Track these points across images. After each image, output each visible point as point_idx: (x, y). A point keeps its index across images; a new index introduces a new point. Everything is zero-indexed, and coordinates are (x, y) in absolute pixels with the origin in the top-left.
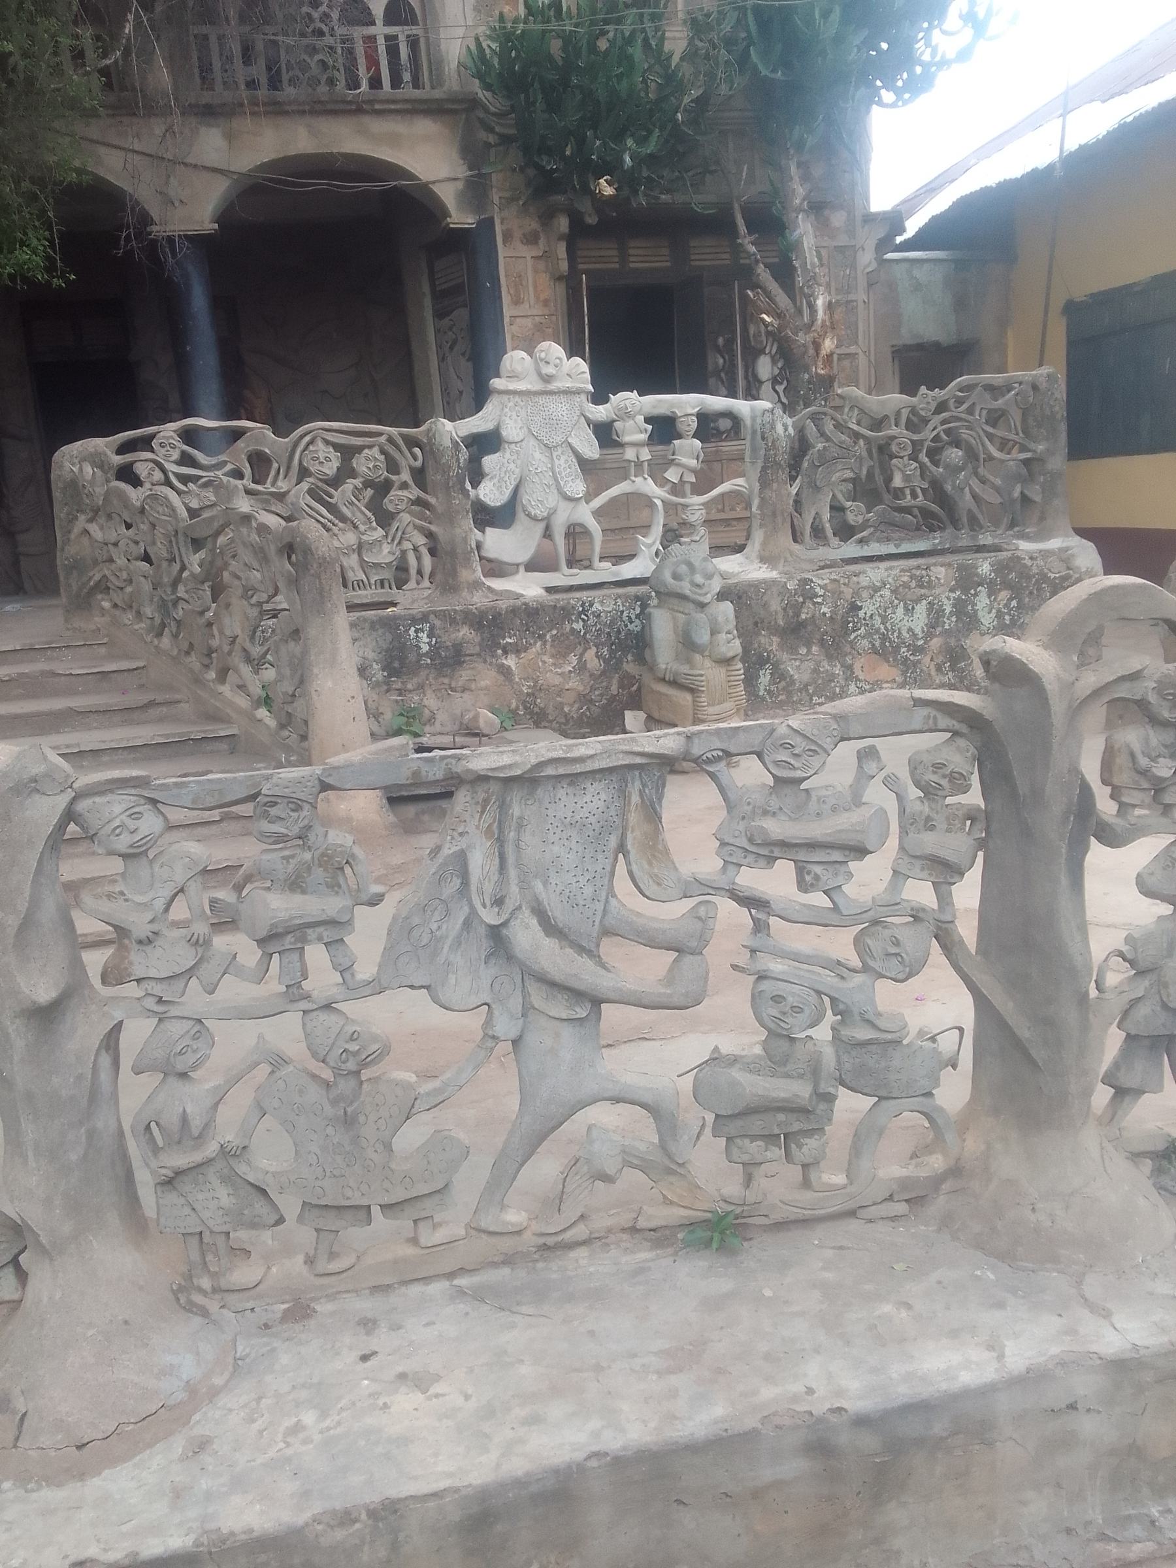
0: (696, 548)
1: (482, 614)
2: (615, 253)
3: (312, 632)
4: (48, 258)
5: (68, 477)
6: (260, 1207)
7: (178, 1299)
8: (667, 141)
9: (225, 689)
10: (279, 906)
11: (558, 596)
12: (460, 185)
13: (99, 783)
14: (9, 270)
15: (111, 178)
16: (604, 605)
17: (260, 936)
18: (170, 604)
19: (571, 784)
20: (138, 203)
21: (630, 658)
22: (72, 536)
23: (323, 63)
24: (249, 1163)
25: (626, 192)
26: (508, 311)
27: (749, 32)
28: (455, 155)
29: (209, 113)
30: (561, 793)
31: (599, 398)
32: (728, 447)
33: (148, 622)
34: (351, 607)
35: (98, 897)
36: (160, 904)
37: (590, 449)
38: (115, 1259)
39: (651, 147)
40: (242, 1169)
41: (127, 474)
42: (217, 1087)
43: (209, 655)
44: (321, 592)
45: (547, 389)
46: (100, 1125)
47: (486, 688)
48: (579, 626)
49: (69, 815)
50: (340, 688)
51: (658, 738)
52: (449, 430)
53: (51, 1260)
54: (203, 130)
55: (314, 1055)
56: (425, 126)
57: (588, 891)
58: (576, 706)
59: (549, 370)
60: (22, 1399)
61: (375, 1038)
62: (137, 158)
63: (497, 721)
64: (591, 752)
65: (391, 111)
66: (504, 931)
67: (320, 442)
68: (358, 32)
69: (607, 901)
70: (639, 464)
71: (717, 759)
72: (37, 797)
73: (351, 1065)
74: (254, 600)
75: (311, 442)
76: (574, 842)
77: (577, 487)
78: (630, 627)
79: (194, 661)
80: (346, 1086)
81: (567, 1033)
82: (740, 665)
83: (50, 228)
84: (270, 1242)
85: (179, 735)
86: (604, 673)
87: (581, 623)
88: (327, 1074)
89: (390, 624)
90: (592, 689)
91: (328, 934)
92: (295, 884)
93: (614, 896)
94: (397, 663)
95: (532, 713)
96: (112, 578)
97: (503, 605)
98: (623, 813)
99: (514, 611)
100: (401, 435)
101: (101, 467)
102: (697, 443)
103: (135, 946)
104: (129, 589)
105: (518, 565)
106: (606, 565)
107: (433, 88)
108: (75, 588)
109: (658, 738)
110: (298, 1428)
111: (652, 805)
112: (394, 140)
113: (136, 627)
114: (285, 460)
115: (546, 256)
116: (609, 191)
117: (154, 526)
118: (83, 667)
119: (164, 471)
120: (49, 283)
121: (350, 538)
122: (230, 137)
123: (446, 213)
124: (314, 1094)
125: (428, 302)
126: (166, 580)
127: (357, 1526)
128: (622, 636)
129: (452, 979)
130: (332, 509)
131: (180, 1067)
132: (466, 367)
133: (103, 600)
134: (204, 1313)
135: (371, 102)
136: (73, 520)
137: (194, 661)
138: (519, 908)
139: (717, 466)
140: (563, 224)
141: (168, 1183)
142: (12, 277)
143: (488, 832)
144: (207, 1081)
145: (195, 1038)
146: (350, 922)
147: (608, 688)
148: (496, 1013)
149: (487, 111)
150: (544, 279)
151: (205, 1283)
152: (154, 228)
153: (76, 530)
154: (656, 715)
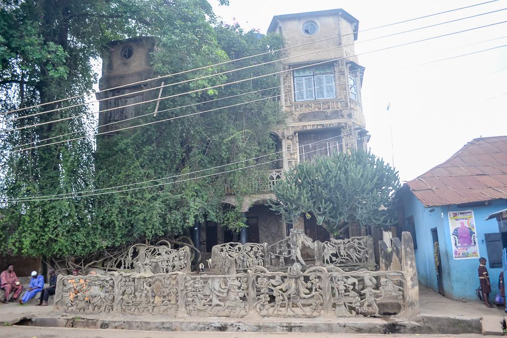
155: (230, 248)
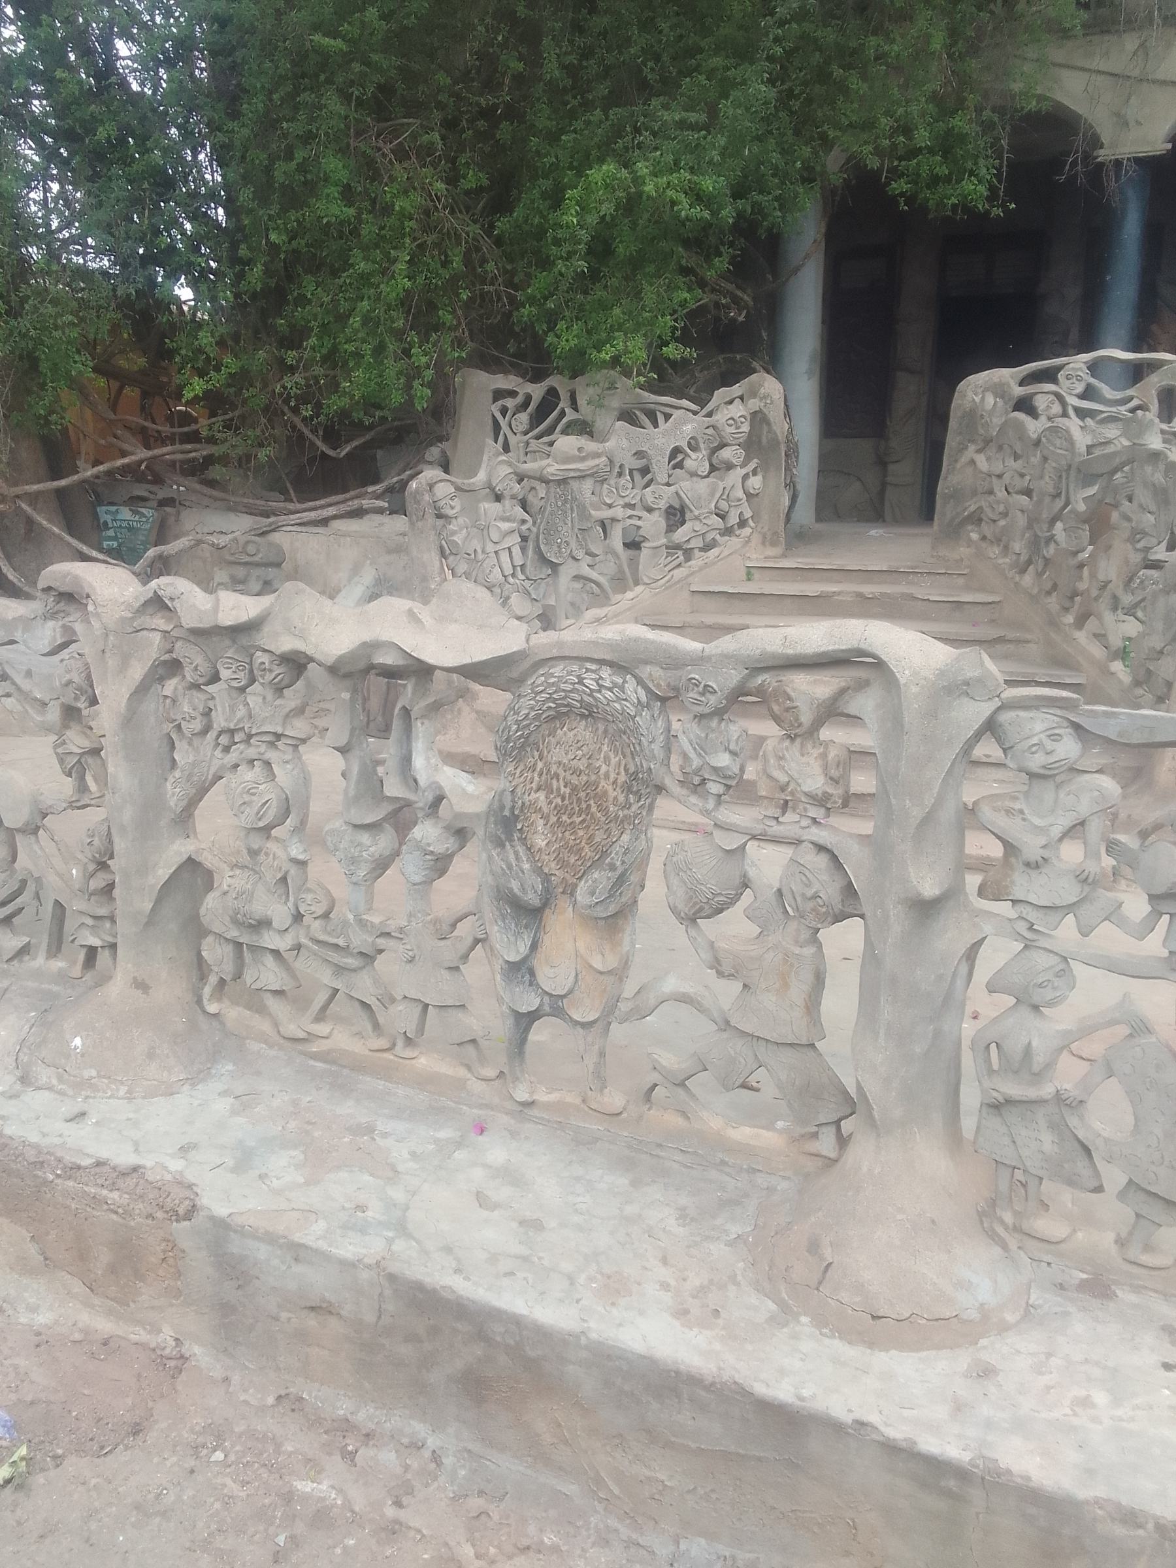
4: (992, 189)
5: (968, 406)
6: (1081, 1165)
7: (982, 1222)
9: (1081, 636)
13: (1028, 697)
14: (954, 200)
15: (1067, 102)
17: (1153, 892)
18: (1043, 541)
20: (1091, 127)
22: (958, 466)
24: (1081, 1118)
33: (1014, 557)
35: (995, 809)
36: (1056, 832)
38: (930, 1158)
40: (1073, 1122)
41: (1025, 405)
43: (1072, 598)
49: (990, 727)
53: (878, 1135)
60: (829, 1250)
72: (965, 700)
74: (1140, 545)
79: (1053, 603)
84: (1070, 1205)
96: (988, 510)
101: (1002, 397)
110: (1086, 1402)
113: (1000, 561)
118: (940, 595)
119: (1064, 403)
120: (988, 212)
127: (1141, 1532)
131: (1036, 999)
133: (972, 531)
134: (1005, 1247)
136: (962, 449)
137: (1053, 603)
142: (954, 206)
145: (1057, 976)
151: (1008, 1218)
152: (1102, 152)
153: (964, 460)
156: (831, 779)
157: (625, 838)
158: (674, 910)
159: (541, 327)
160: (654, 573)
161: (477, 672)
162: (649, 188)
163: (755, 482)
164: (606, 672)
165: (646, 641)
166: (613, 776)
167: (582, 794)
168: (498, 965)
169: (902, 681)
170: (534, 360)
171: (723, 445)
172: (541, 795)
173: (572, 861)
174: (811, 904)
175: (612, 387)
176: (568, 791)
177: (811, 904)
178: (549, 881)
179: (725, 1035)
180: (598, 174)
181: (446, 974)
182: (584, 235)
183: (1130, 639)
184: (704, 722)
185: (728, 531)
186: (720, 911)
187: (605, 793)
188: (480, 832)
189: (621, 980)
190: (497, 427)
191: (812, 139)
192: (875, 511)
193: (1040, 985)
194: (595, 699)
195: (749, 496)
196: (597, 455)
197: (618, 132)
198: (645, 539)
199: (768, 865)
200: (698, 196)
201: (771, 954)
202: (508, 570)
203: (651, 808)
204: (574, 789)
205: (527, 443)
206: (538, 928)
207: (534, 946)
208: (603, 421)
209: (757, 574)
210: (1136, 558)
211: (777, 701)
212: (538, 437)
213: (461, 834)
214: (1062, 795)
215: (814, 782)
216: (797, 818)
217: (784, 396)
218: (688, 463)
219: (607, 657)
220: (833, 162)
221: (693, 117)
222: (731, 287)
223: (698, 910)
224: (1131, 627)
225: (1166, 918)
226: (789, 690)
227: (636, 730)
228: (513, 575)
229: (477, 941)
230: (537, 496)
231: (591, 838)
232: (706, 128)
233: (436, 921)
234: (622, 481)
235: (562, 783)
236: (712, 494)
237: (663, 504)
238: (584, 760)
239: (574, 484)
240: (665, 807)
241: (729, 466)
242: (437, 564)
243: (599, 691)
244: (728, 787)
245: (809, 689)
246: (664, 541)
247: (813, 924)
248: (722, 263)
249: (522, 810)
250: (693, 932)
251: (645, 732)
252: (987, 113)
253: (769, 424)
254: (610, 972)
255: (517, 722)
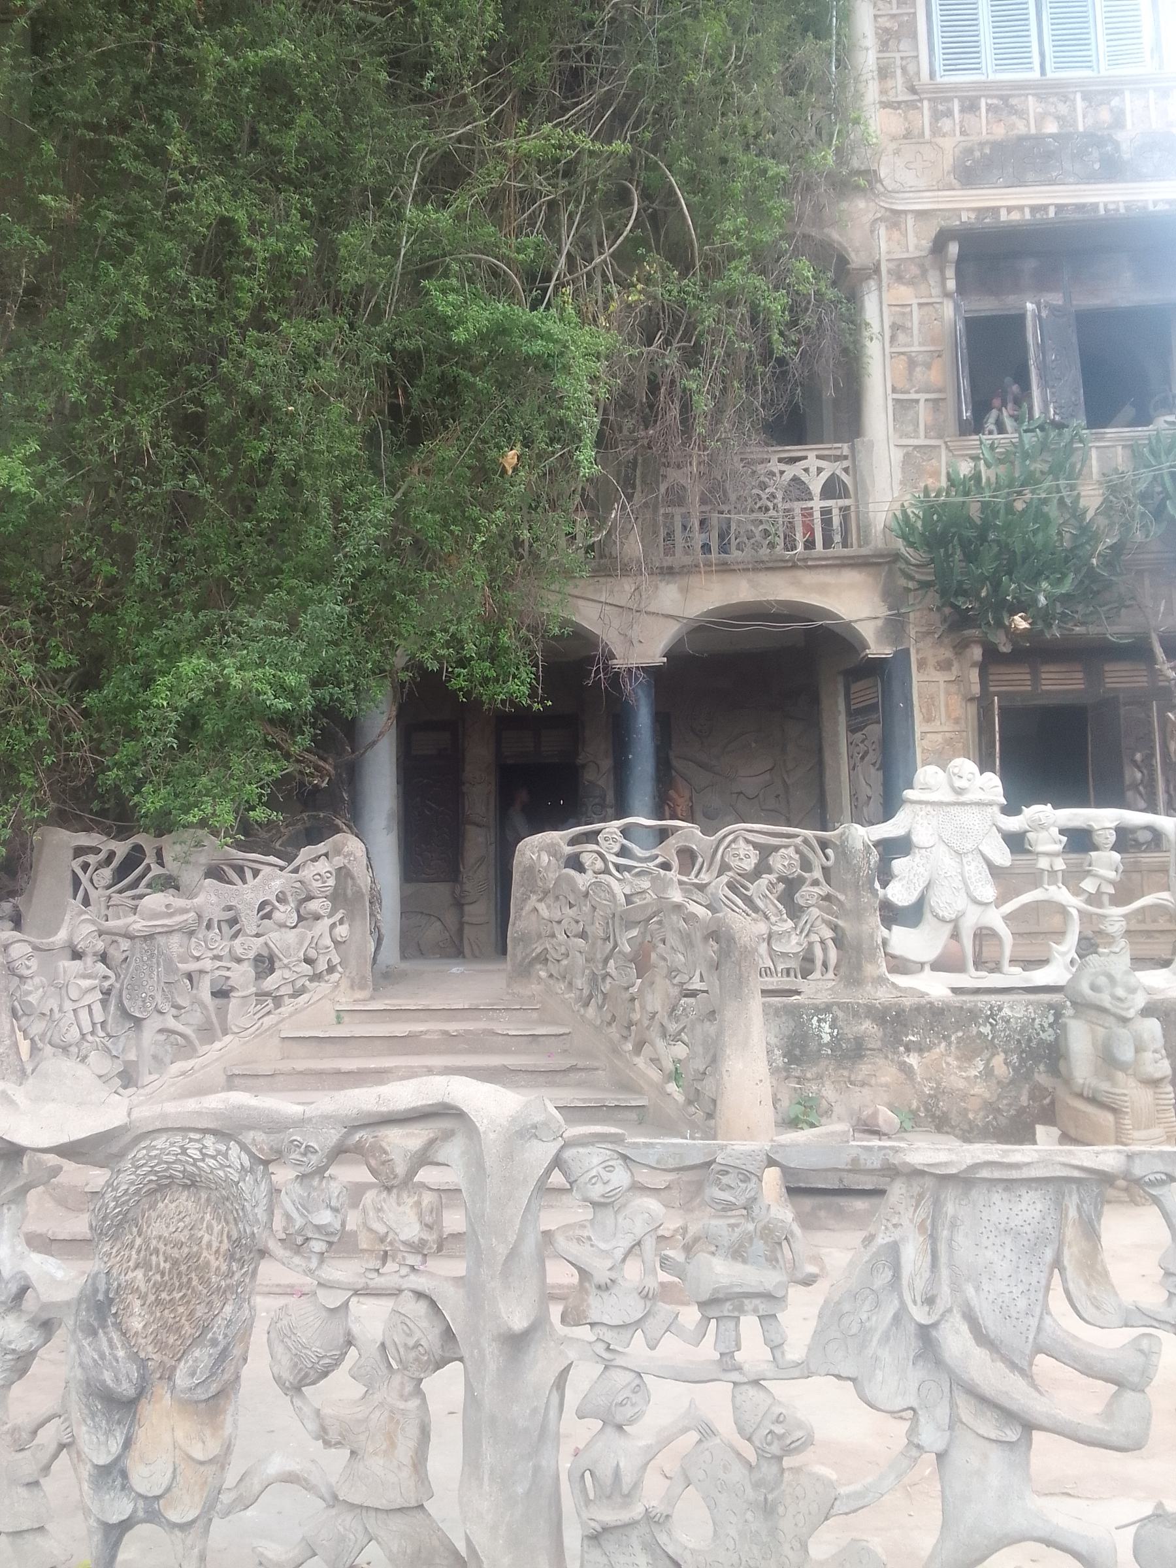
0: (1116, 959)
1: (886, 1009)
2: (1028, 677)
3: (729, 1014)
4: (533, 689)
5: (527, 863)
8: (1082, 582)
9: (640, 1061)
10: (721, 1271)
11: (964, 998)
12: (880, 623)
13: (585, 1135)
16: (1014, 1010)
19: (1006, 1189)
21: (1042, 1067)
23: (766, 533)
24: (669, 1534)
25: (1040, 626)
26: (919, 727)
27: (1163, 485)
28: (877, 599)
29: (669, 572)
30: (996, 1197)
31: (1010, 810)
32: (1148, 858)
34: (765, 993)
36: (619, 1254)
37: (1002, 856)
39: (1066, 587)
40: (663, 1538)
41: (575, 863)
42: (649, 1447)
43: (628, 1028)
44: (740, 978)
45: (959, 800)
46: (544, 1463)
47: (887, 1085)
48: (986, 1030)
49: (557, 1162)
50: (749, 1072)
51: (1097, 1154)
52: (862, 835)
54: (662, 585)
55: (741, 1430)
56: (851, 576)
57: (1022, 1303)
58: (982, 1114)
59: (958, 783)
61: (800, 1425)
62: (608, 608)
63: (897, 1120)
64: (1027, 1160)
65: (826, 566)
66: (934, 1333)
67: (741, 841)
68: (798, 506)
69: (1041, 1318)
70: (1052, 872)
71: (1161, 1183)
72: (535, 1142)
73: (775, 1449)
74: (676, 981)
75: (734, 841)
76: (1008, 1250)
77: (988, 892)
78: (1043, 1035)
79: (614, 1032)
80: (768, 1471)
81: (996, 1455)
82: (1170, 1089)
83: (536, 665)
85: (596, 1100)
86: (1012, 1082)
87: (989, 1027)
88: (752, 1457)
89: (794, 1012)
90: (1000, 1097)
91: (763, 1307)
92: (738, 1253)
93: (1049, 1313)
94: (797, 1051)
95: (933, 1116)
97: (908, 1002)
98: (1060, 1227)
99: (918, 1009)
100: (817, 838)
101: (554, 856)
102: (1116, 856)
103: (594, 1291)
104: (565, 962)
105: (922, 964)
106: (1018, 970)
107: (860, 546)
108: (519, 958)
109: (1097, 1154)
111: (1090, 1222)
112: (823, 589)
114: (709, 855)
115: (958, 680)
116: (1023, 625)
117: (594, 908)
120: (530, 707)
121: (762, 928)
122: (685, 591)
123: (865, 646)
124: (738, 1473)
125: (842, 719)
126: (599, 956)
128: (1034, 1044)
129: (879, 1375)
130: (748, 901)
131: (619, 1419)
132: (877, 776)
135: (805, 560)
136: (525, 899)
137: (614, 1032)
138: (950, 1310)
139: (1136, 877)
140: (977, 653)
141: (596, 1537)
142: (503, 702)
143: (921, 1227)
144: (643, 1433)
145: (634, 1392)
146: (783, 1299)
147: (1017, 1098)
148: (922, 1420)
149: (908, 563)
150: (956, 701)
153: (528, 908)
154: (1072, 1132)
155: (623, 852)
156: (427, 1225)
157: (228, 1309)
158: (278, 1380)
159: (127, 790)
160: (244, 1022)
161: (71, 1151)
162: (236, 682)
163: (342, 931)
164: (209, 1141)
165: (249, 1108)
166: (215, 1245)
167: (183, 1268)
168: (86, 1471)
169: (482, 1129)
170: (118, 817)
171: (310, 898)
172: (139, 1274)
173: (171, 1341)
174: (413, 1354)
175: (199, 844)
176: (168, 1265)
177: (413, 1354)
178: (145, 1367)
179: (333, 1512)
180: (191, 665)
181: (23, 1492)
182: (174, 716)
183: (680, 1061)
184: (306, 1181)
185: (316, 977)
186: (325, 1374)
187: (208, 1263)
188: (70, 1322)
189: (223, 1468)
190: (77, 883)
191: (381, 644)
192: (455, 947)
193: (621, 1404)
194: (198, 1168)
195: (337, 943)
196: (185, 911)
197: (207, 631)
198: (233, 989)
199: (371, 1320)
200: (283, 690)
201: (377, 1413)
202: (87, 1028)
203: (254, 1273)
204: (175, 1263)
205: (110, 898)
206: (133, 1421)
207: (127, 1444)
208: (190, 876)
209: (346, 1018)
210: (675, 992)
211: (374, 1156)
212: (120, 892)
213: (46, 1326)
214: (620, 1220)
215: (411, 1230)
216: (396, 1267)
217: (367, 851)
218: (276, 915)
219: (211, 1126)
220: (399, 660)
221: (276, 625)
222: (314, 758)
223: (301, 1380)
224: (680, 1051)
225: (713, 1322)
226: (384, 1144)
227: (239, 1197)
228: (93, 1033)
229: (62, 1446)
230: (118, 948)
231: (192, 1313)
232: (288, 633)
233: (15, 1429)
234: (211, 935)
235: (161, 1258)
236: (301, 943)
237: (252, 955)
238: (186, 1232)
239: (161, 940)
240: (269, 1272)
241: (317, 917)
242: (8, 1027)
243: (203, 1160)
244: (330, 1244)
245: (402, 1142)
246: (253, 990)
247: (416, 1375)
248: (303, 741)
249: (117, 1293)
250: (298, 1402)
251: (248, 1197)
252: (524, 631)
253: (353, 878)
254: (211, 1461)
255: (116, 1199)
